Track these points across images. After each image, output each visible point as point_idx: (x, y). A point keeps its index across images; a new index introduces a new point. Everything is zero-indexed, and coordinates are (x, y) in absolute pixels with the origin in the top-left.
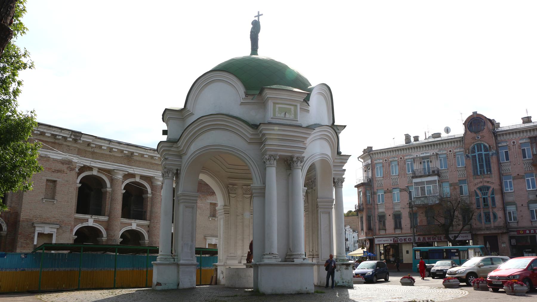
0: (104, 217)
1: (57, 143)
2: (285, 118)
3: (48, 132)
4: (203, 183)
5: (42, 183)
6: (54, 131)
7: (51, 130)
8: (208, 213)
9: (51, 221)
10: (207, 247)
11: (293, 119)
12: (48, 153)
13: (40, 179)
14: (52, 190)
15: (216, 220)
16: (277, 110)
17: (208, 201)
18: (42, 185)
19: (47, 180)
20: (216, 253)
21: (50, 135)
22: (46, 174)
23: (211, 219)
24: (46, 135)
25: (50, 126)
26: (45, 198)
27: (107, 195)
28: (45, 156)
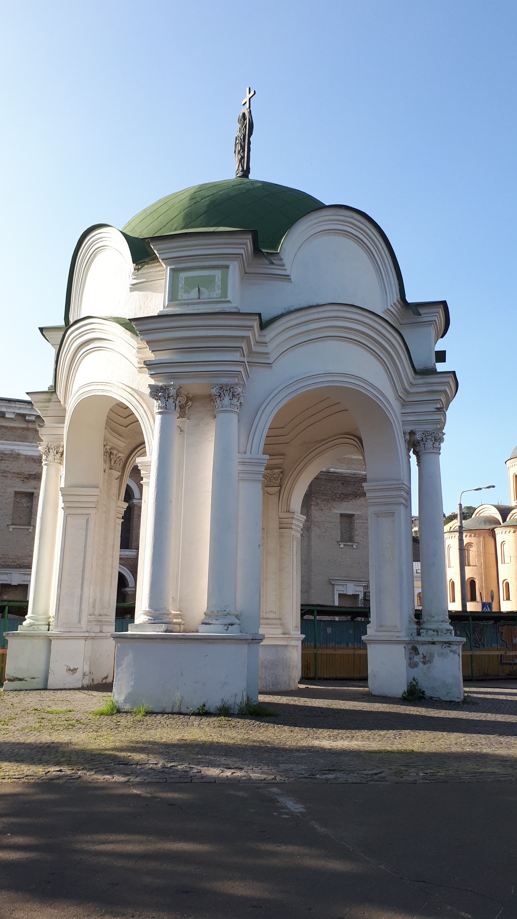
0: (129, 551)
1: (32, 428)
2: (199, 301)
3: (9, 410)
4: (322, 477)
5: (6, 500)
6: (20, 408)
7: (13, 407)
8: (336, 533)
9: (24, 563)
10: (337, 604)
11: (220, 300)
12: (16, 448)
13: (3, 493)
14: (28, 509)
15: (355, 547)
16: (180, 285)
17: (336, 511)
18: (7, 501)
19: (16, 493)
20: (366, 613)
21: (13, 416)
22: (13, 483)
23: (342, 546)
24: (7, 416)
25: (9, 401)
26: (12, 524)
27: (135, 511)
28: (10, 452)
